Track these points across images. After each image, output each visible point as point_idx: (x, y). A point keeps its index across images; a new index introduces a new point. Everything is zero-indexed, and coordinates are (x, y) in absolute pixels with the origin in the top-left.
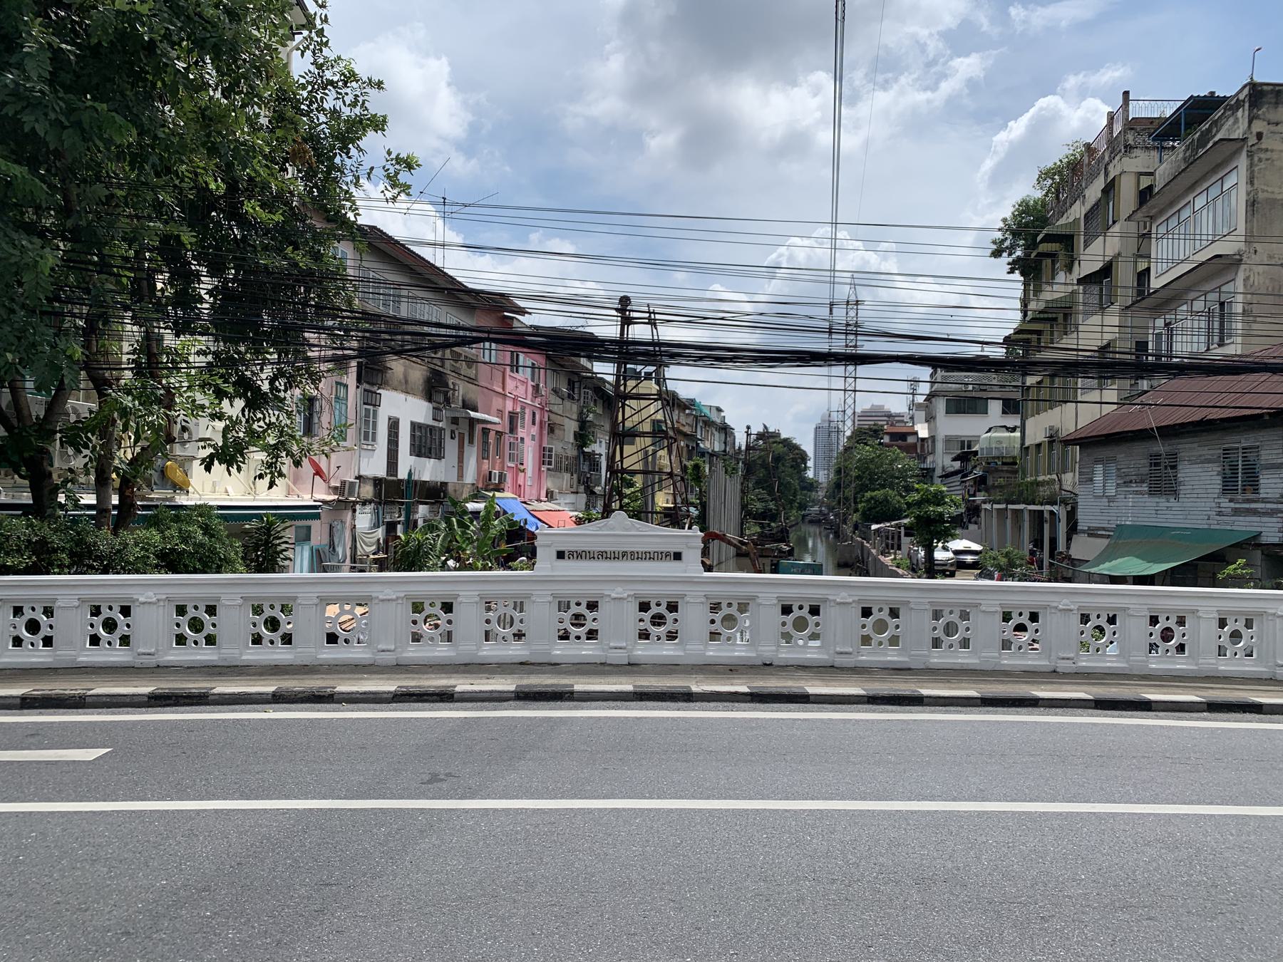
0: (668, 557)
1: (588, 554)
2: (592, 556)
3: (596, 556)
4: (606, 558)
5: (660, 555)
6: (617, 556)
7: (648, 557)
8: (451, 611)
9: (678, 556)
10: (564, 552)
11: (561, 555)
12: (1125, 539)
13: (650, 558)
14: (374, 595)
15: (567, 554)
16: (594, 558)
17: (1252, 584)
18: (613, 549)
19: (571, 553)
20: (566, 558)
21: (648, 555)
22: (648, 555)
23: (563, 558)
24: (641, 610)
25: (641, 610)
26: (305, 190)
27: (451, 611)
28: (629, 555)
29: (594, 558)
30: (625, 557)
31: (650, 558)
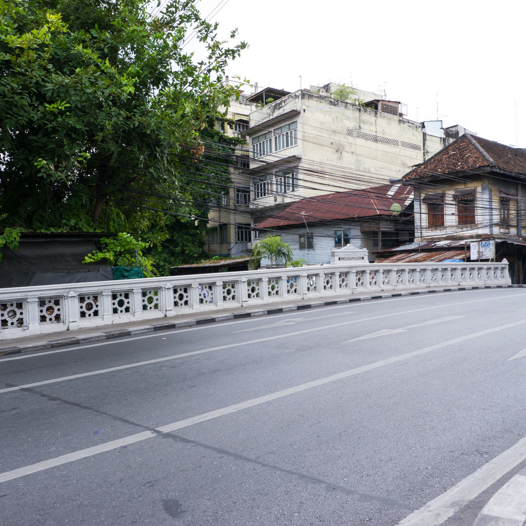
8: (41, 316)
14: (301, 275)
24: (85, 316)
25: (85, 316)
27: (41, 316)
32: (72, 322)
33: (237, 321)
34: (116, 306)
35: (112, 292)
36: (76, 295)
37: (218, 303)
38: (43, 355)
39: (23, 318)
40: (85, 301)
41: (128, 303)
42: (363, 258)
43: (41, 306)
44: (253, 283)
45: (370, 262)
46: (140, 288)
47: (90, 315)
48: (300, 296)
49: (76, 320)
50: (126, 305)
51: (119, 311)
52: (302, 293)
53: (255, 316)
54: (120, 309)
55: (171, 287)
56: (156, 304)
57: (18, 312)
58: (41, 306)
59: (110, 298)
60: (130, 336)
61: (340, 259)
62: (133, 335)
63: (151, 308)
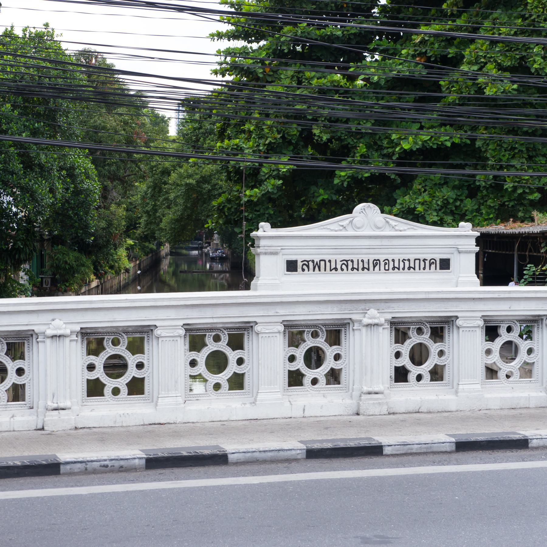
0: (433, 266)
1: (328, 264)
2: (333, 266)
3: (339, 267)
4: (353, 269)
5: (422, 263)
6: (396, 265)
7: (350, 267)
8: (397, 369)
9: (445, 264)
10: (296, 262)
11: (292, 266)
12: (229, 139)
13: (409, 268)
14: (37, 329)
15: (300, 264)
16: (336, 269)
17: (370, 199)
18: (360, 257)
19: (306, 263)
20: (299, 269)
21: (407, 263)
22: (407, 263)
23: (295, 270)
24: (300, 384)
25: (300, 384)
26: (388, 137)
27: (397, 369)
28: (382, 264)
29: (336, 269)
30: (377, 268)
31: (409, 268)
32: (370, 393)
33: (177, 479)
34: (300, 364)
35: (486, 320)
36: (382, 320)
37: (461, 387)
38: (69, 497)
39: (243, 375)
40: (205, 345)
41: (240, 361)
42: (445, 264)
43: (90, 352)
44: (509, 329)
45: (485, 282)
46: (480, 314)
47: (419, 378)
48: (348, 401)
49: (68, 404)
50: (329, 364)
51: (412, 377)
52: (41, 403)
53: (71, 474)
54: (110, 383)
55: (382, 320)
56: (332, 370)
57: (232, 356)
58: (90, 352)
59: (480, 335)
60: (224, 468)
61: (292, 266)
62: (537, 448)
63: (419, 378)
